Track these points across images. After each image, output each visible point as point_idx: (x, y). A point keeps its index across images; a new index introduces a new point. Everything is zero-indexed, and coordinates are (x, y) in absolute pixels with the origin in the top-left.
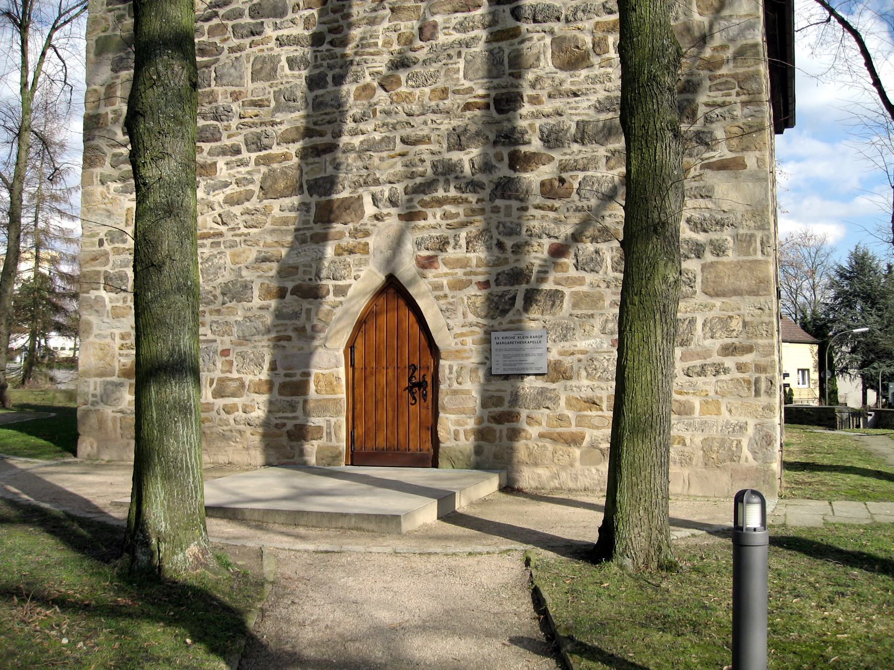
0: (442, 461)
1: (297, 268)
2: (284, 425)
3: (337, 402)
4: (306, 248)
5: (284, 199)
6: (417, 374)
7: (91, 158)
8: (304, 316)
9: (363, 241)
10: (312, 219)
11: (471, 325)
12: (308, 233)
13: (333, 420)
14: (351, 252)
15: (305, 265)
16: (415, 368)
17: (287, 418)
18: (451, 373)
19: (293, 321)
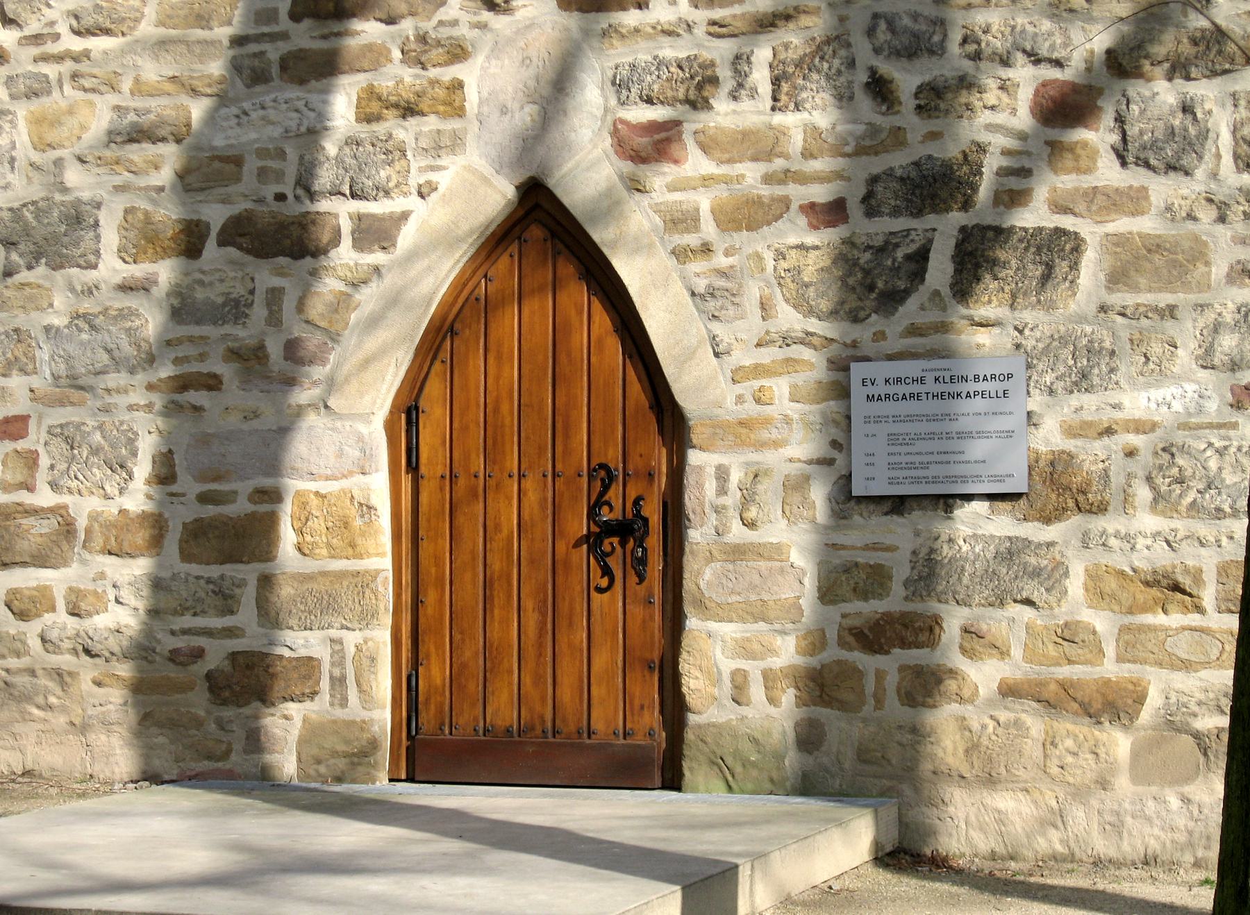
1: (237, 161)
2: (198, 654)
3: (362, 581)
4: (268, 99)
6: (614, 495)
8: (259, 312)
11: (787, 340)
12: (274, 52)
13: (352, 639)
14: (409, 110)
15: (262, 153)
17: (208, 633)
18: (722, 491)
19: (227, 329)
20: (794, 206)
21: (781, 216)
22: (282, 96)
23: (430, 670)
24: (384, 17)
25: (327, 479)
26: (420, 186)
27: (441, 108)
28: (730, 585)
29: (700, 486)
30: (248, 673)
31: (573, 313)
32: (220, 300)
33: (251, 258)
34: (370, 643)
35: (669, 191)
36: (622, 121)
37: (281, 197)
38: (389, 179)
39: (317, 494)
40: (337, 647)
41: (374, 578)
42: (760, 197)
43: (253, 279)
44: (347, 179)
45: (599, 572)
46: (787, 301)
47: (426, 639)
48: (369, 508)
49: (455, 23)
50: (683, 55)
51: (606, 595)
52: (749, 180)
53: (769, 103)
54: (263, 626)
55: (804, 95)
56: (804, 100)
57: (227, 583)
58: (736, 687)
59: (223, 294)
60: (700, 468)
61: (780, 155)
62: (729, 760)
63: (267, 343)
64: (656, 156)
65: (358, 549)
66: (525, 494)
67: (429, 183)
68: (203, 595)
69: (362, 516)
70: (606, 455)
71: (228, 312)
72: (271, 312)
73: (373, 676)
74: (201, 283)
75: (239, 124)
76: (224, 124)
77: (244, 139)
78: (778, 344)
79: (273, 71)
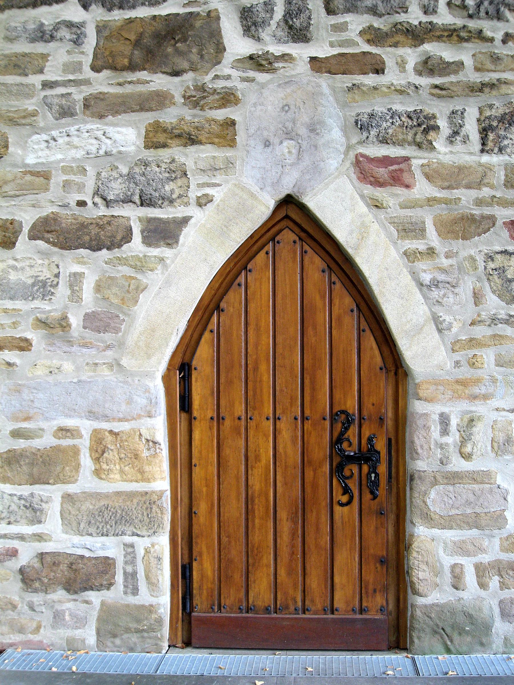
0: (421, 639)
1: (46, 176)
2: (13, 553)
3: (149, 500)
4: (72, 130)
5: (15, 12)
6: (352, 433)
7: (287, 520)
8: (62, 291)
9: (220, 114)
10: (88, 60)
11: (494, 320)
12: (78, 95)
13: (141, 544)
14: (191, 140)
15: (66, 170)
16: (348, 422)
17: (22, 538)
18: (445, 432)
19: (37, 303)
20: (499, 223)
21: (488, 230)
22: (89, 126)
23: (202, 565)
24: (169, 70)
25: (120, 420)
26: (198, 198)
27: (216, 140)
28: (451, 502)
29: (427, 428)
30: (55, 568)
31: (318, 297)
32: (30, 281)
33: (56, 249)
34: (156, 547)
35: (401, 208)
36: (362, 155)
37: (82, 204)
38: (172, 191)
39: (111, 432)
40: (130, 550)
41: (160, 497)
42: (472, 215)
43: (58, 266)
44: (137, 191)
45: (340, 491)
46: (494, 292)
47: (199, 541)
48: (155, 443)
49: (228, 77)
50: (411, 109)
51: (346, 509)
52: (463, 202)
53: (478, 147)
54: (67, 533)
55: (506, 142)
56: (507, 146)
57: (36, 500)
58: (455, 577)
59: (32, 277)
60: (426, 415)
61: (488, 185)
62: (448, 630)
63: (69, 315)
64: (392, 182)
65: (146, 475)
66: (280, 433)
67: (206, 195)
68: (16, 509)
69: (149, 449)
70: (345, 403)
71: (37, 291)
72: (73, 291)
73: (159, 572)
74: (14, 268)
75: (48, 147)
76: (36, 147)
77: (52, 159)
78: (487, 323)
79: (77, 107)
